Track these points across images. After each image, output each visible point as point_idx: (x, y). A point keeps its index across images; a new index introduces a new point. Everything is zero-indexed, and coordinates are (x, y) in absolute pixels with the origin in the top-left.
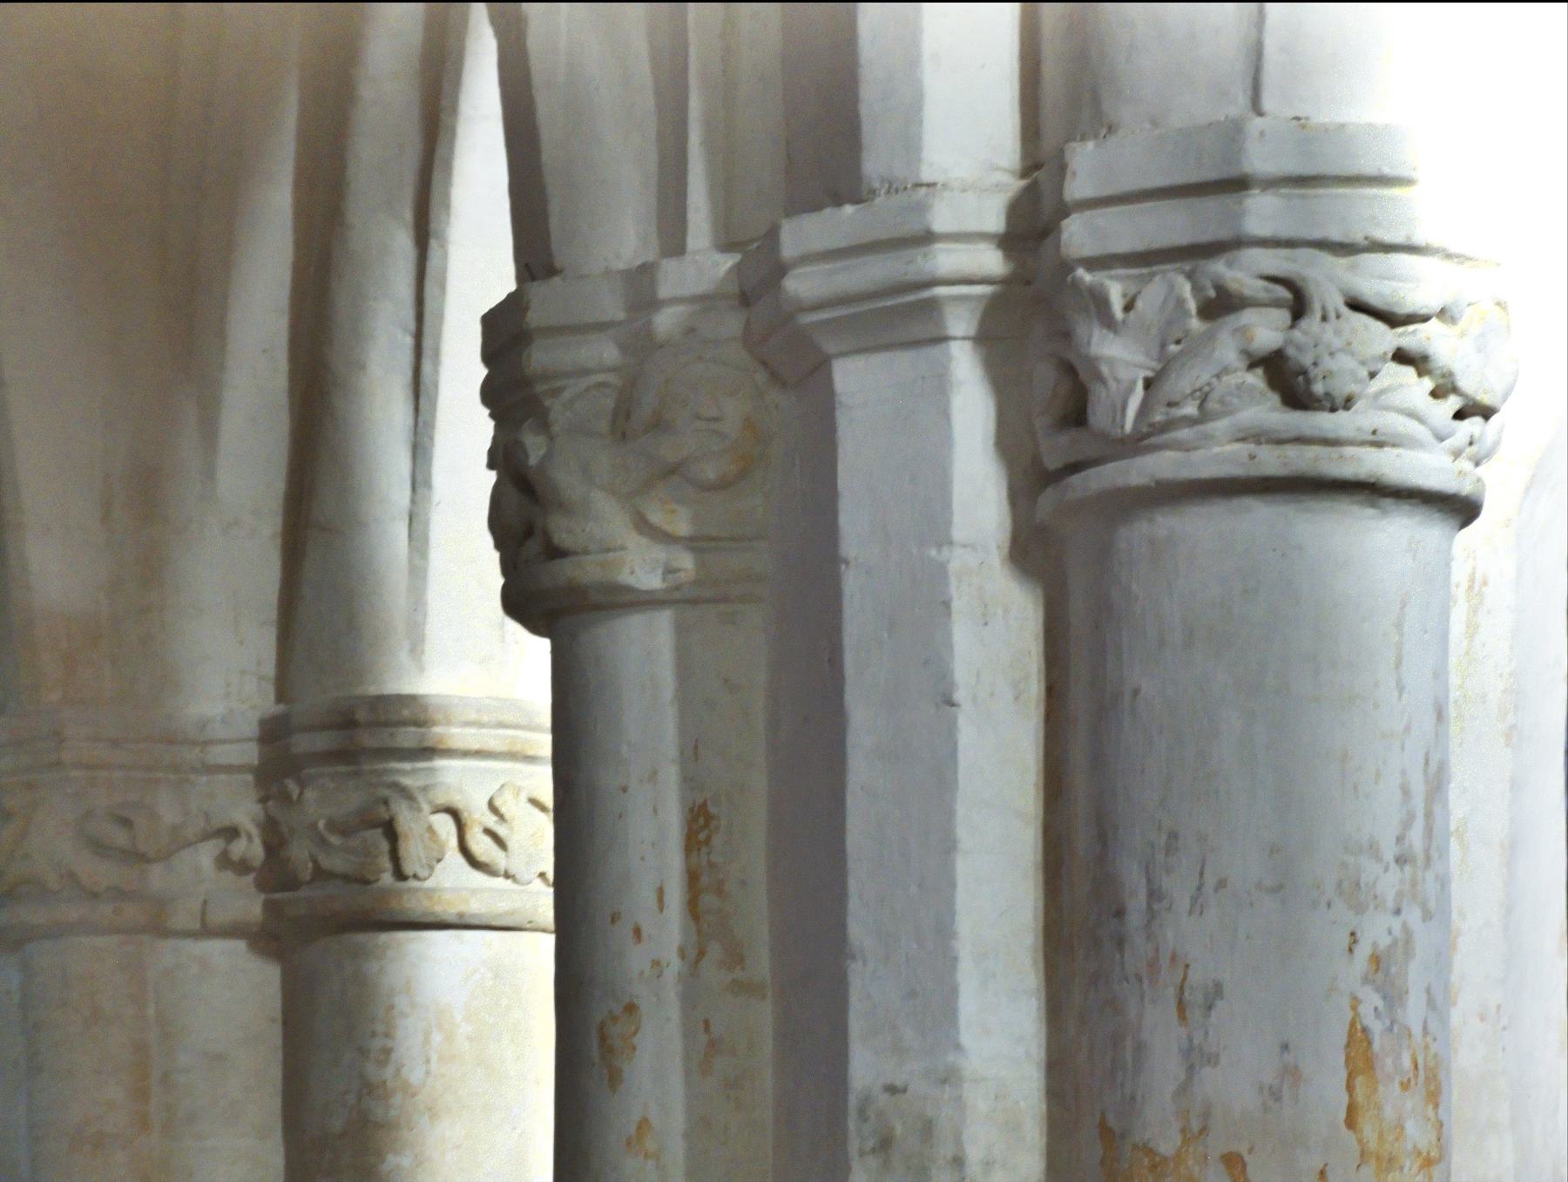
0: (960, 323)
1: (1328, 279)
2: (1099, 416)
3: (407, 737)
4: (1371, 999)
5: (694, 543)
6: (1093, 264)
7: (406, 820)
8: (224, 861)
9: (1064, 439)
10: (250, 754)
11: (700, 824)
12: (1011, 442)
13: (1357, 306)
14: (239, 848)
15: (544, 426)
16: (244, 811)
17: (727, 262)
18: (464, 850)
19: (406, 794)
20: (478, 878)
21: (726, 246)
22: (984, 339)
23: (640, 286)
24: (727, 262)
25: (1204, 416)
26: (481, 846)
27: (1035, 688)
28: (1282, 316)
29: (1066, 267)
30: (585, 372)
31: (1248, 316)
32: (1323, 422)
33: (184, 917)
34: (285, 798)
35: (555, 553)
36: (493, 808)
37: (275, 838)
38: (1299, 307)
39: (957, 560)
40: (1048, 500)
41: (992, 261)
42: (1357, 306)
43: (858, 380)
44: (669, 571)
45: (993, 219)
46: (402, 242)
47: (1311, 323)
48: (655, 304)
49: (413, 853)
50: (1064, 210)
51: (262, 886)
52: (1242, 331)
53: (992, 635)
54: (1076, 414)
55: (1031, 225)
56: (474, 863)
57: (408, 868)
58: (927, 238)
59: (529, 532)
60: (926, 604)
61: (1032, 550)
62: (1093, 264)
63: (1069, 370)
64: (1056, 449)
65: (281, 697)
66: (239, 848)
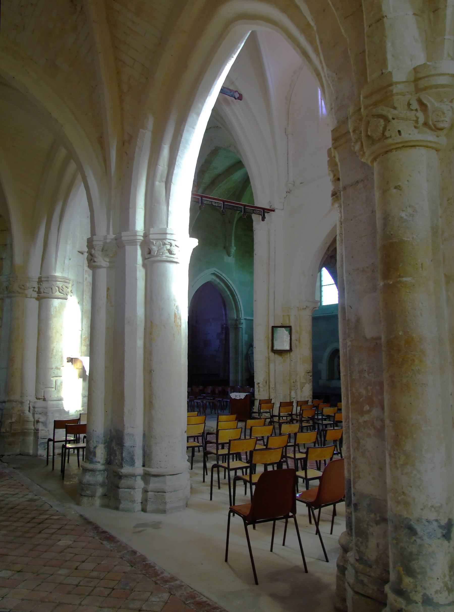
0: (139, 244)
1: (174, 243)
2: (152, 253)
3: (54, 279)
4: (176, 310)
5: (109, 262)
6: (152, 239)
7: (53, 288)
8: (33, 290)
9: (149, 255)
10: (37, 280)
11: (108, 289)
12: (143, 255)
13: (176, 246)
14: (35, 289)
15: (94, 250)
16: (36, 286)
17: (115, 236)
18: (59, 291)
19: (53, 285)
20: (60, 294)
21: (114, 234)
22: (140, 246)
23: (105, 238)
24: (115, 236)
25: (163, 254)
26: (61, 291)
27: (144, 279)
28: (169, 246)
29: (150, 239)
30: (99, 245)
31: (167, 246)
32: (172, 256)
33: (29, 296)
34: (41, 285)
35: (94, 262)
36: (62, 287)
37: (39, 288)
38: (171, 245)
39: (138, 266)
40: (146, 261)
41: (142, 238)
42: (176, 246)
43: (128, 248)
44: (106, 265)
45: (142, 235)
46: (56, 232)
47: (172, 247)
48: (107, 239)
49: (54, 291)
50: (149, 234)
51: (37, 293)
52: (166, 247)
53: (141, 273)
54: (150, 253)
55: (146, 235)
56: (60, 292)
57: (53, 292)
58: (166, 234)
59: (91, 260)
60: (135, 270)
61: (144, 265)
62: (152, 239)
63: (149, 249)
64: (147, 256)
65: (40, 274)
66: (35, 289)
